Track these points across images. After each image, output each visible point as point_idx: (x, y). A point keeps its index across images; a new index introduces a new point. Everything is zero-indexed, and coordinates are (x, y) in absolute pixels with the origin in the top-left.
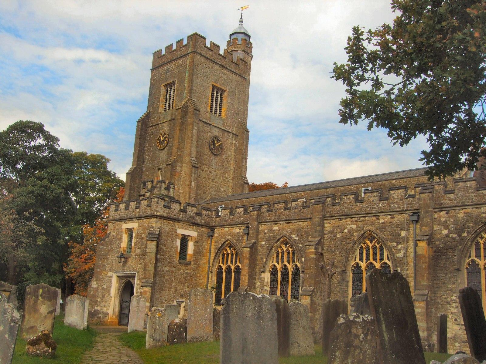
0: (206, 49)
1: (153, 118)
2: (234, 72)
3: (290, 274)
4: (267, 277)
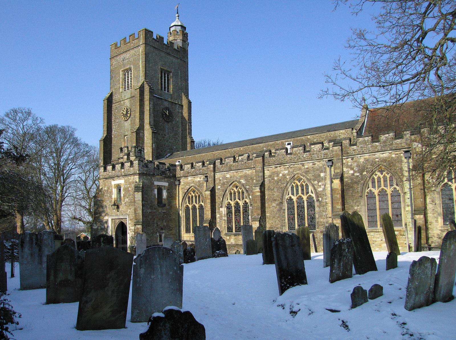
3: (241, 207)
4: (223, 210)
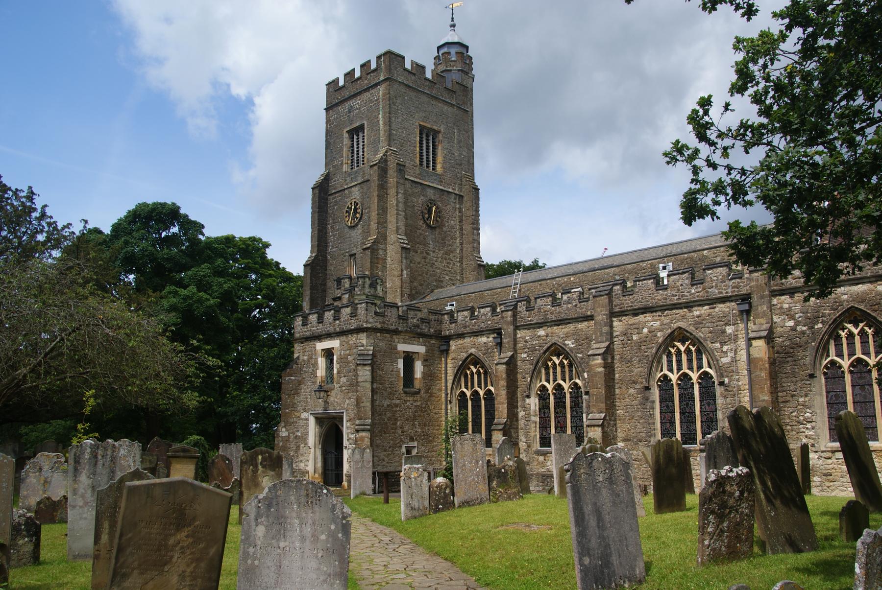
1: (335, 181)
2: (449, 103)
3: (568, 396)
4: (533, 403)
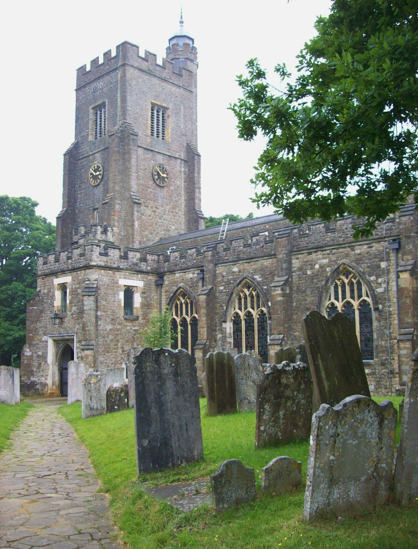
0: (139, 59)
1: (82, 149)
2: (177, 85)
3: (256, 321)
4: (229, 327)
